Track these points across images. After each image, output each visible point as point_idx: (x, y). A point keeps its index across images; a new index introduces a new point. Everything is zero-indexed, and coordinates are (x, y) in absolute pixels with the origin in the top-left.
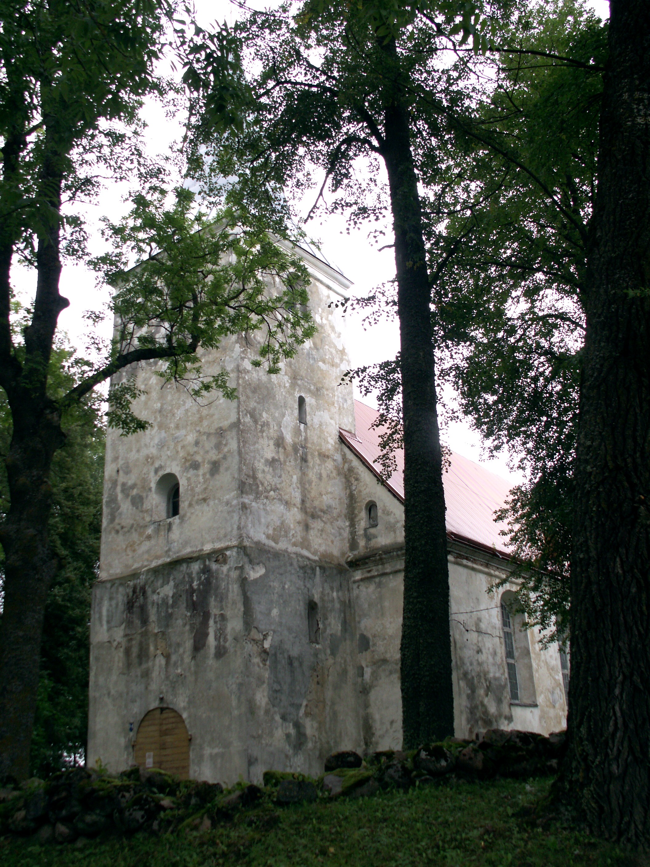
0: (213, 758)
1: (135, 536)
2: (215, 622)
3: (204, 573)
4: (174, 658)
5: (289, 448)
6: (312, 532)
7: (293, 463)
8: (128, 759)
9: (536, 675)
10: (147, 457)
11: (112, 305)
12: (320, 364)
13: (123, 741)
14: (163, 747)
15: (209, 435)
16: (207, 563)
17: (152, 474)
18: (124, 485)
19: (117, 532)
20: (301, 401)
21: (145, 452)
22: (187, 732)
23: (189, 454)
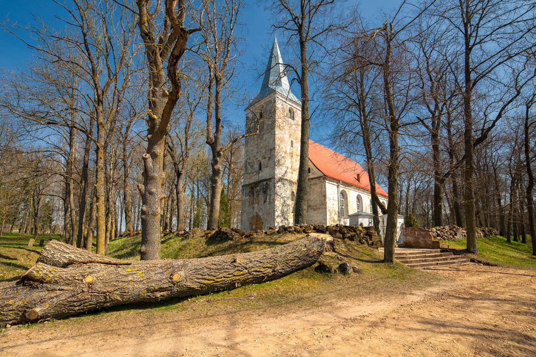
1: (251, 175)
13: (248, 223)
14: (257, 224)
20: (292, 142)
21: (253, 154)
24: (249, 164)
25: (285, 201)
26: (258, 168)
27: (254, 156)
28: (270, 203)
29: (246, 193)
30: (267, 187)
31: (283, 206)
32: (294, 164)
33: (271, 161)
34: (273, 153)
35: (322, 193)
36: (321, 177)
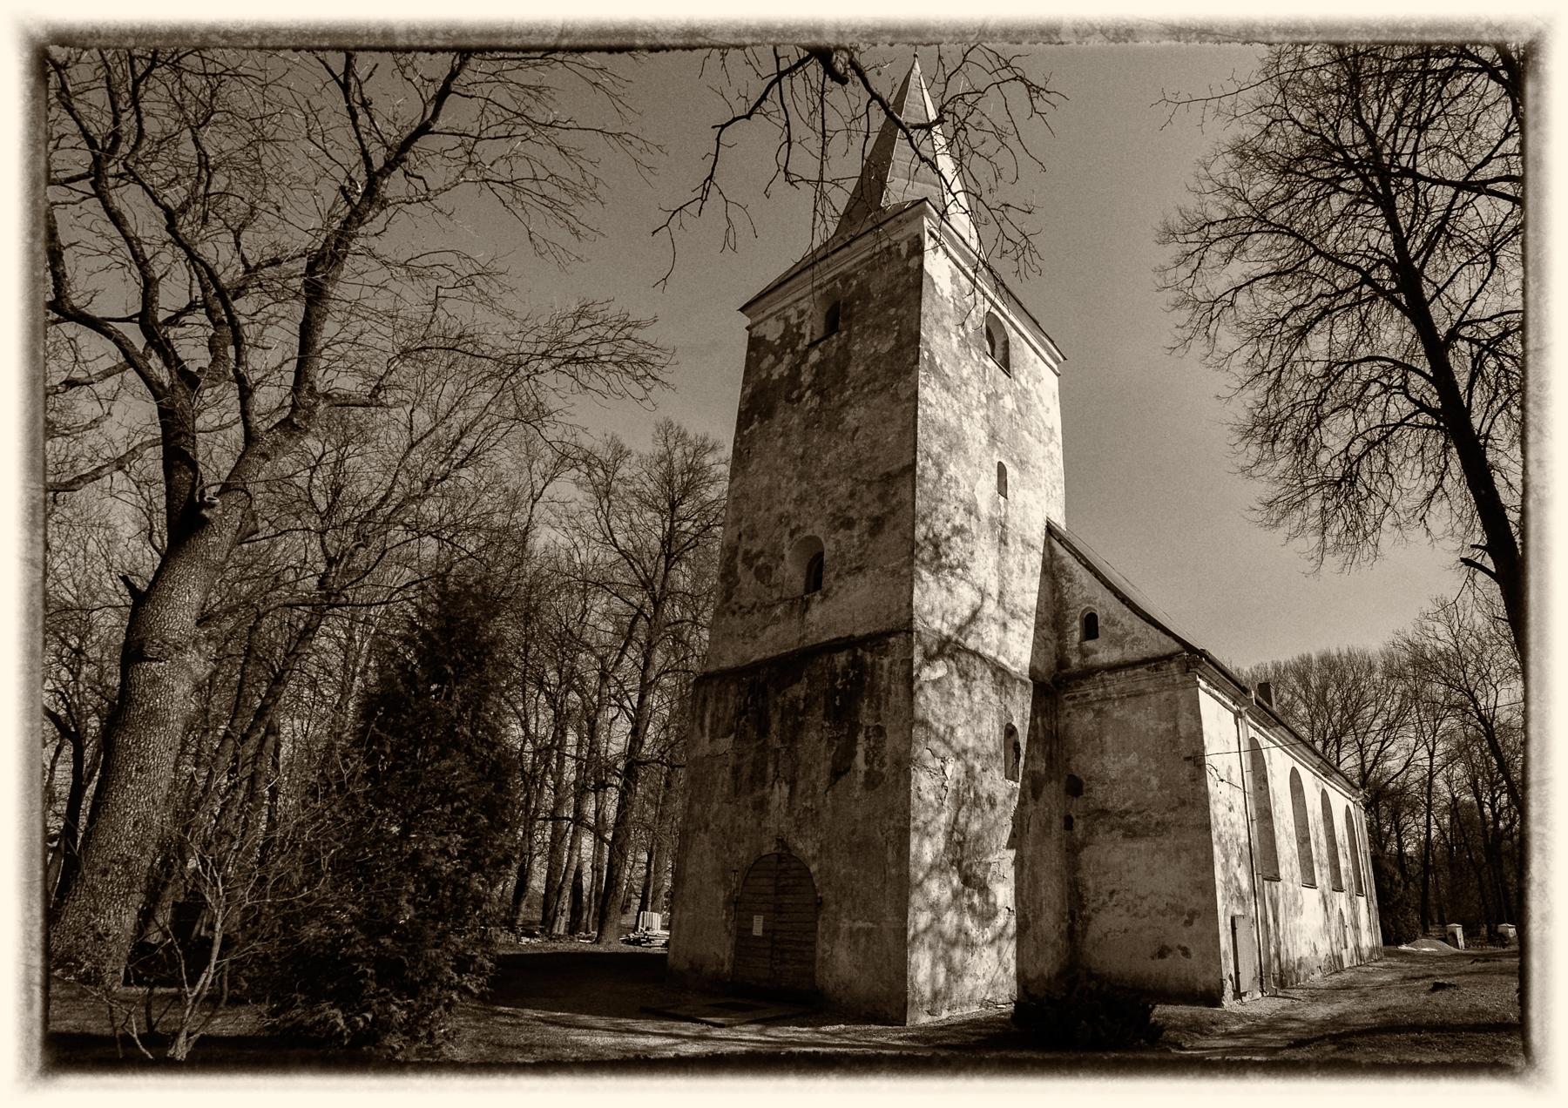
0: (852, 934)
1: (756, 617)
2: (868, 738)
3: (853, 668)
4: (801, 785)
5: (984, 521)
6: (1010, 635)
7: (988, 540)
9: (1278, 843)
10: (781, 516)
11: (818, 597)
12: (1025, 433)
13: (721, 895)
15: (870, 483)
16: (860, 652)
17: (786, 537)
18: (747, 552)
19: (734, 613)
20: (1002, 470)
21: (778, 510)
22: (816, 892)
23: (839, 509)
24: (749, 559)
25: (969, 771)
26: (799, 584)
27: (783, 519)
28: (872, 781)
29: (716, 720)
30: (859, 681)
31: (959, 802)
32: (1014, 585)
33: (889, 537)
34: (905, 494)
35: (1175, 743)
36: (1169, 658)
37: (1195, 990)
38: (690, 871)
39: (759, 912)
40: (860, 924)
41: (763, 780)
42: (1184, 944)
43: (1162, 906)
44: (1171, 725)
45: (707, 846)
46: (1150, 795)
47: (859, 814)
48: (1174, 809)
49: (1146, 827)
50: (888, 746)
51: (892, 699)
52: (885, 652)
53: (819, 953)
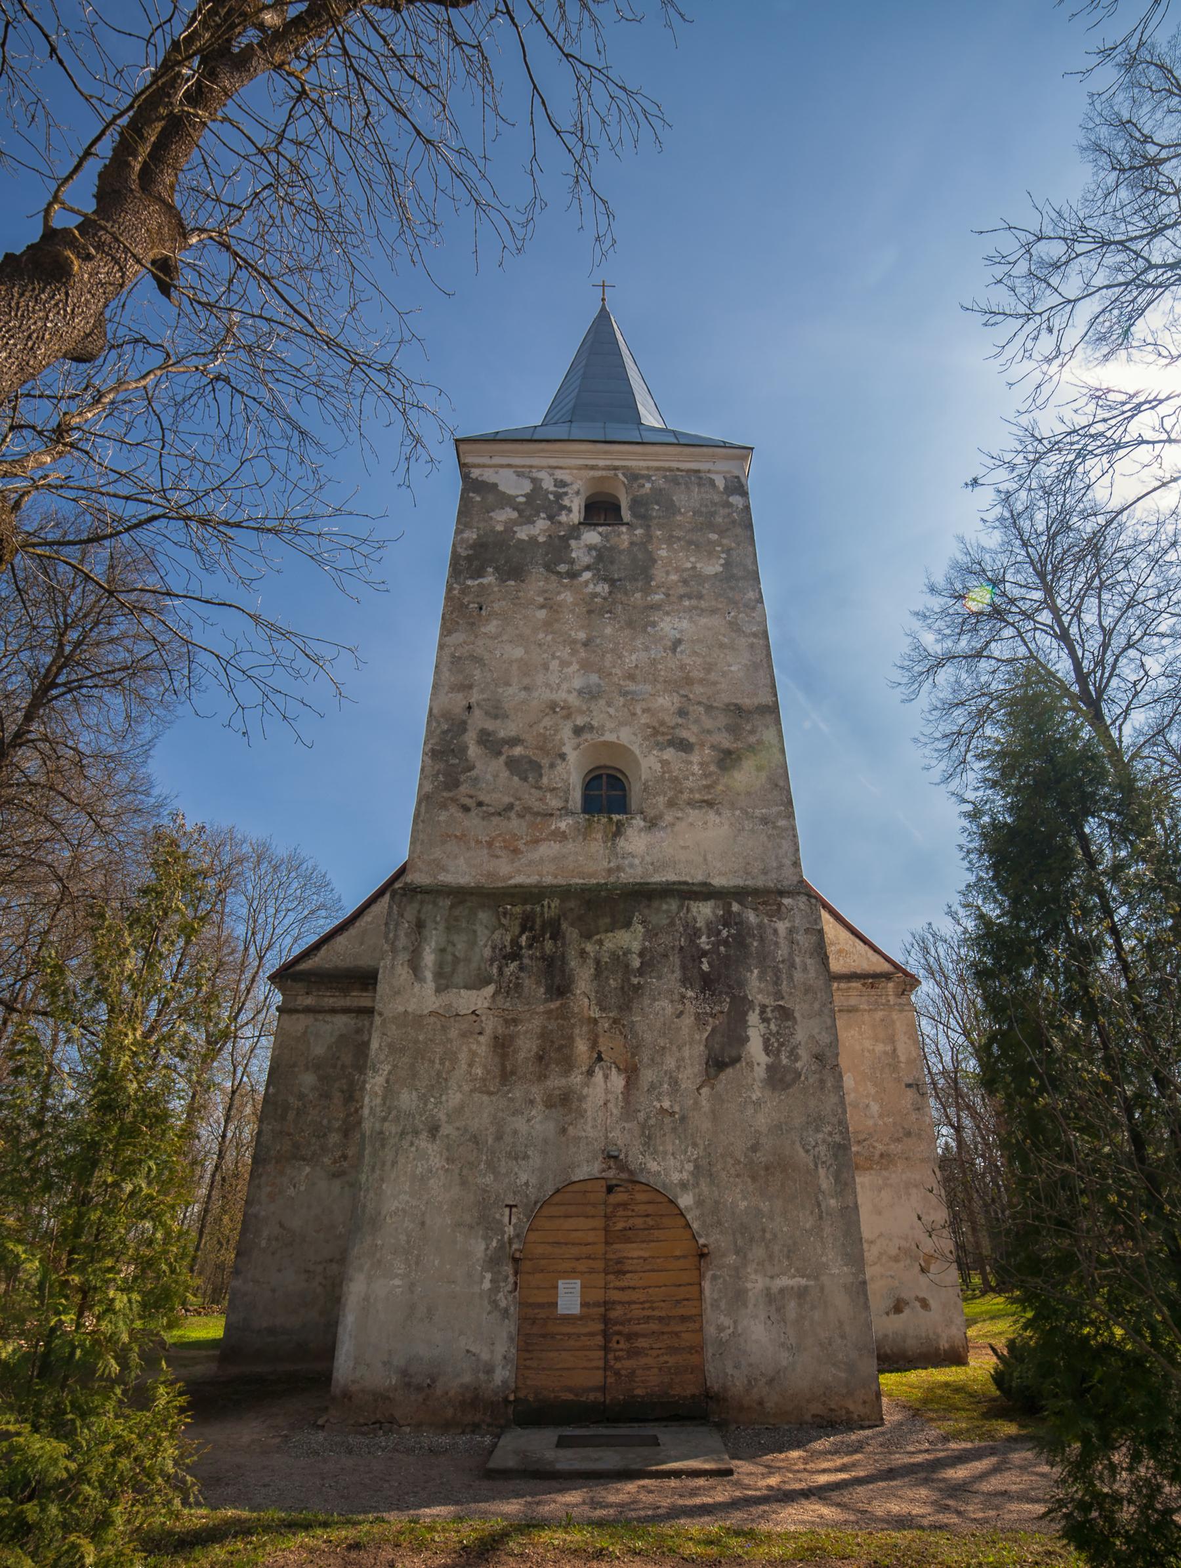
0: (773, 1299)
2: (765, 1020)
3: (726, 925)
4: (648, 1076)
8: (495, 1289)
13: (479, 1249)
35: (895, 1068)
36: (887, 976)
37: (937, 1349)
38: (394, 1205)
39: (571, 1273)
40: (784, 1281)
41: (568, 1064)
42: (921, 1295)
43: (893, 1251)
44: (889, 1048)
45: (437, 1162)
46: (870, 1123)
47: (762, 1121)
48: (899, 1140)
49: (869, 1158)
50: (800, 1035)
51: (798, 975)
52: (778, 912)
53: (711, 1330)
